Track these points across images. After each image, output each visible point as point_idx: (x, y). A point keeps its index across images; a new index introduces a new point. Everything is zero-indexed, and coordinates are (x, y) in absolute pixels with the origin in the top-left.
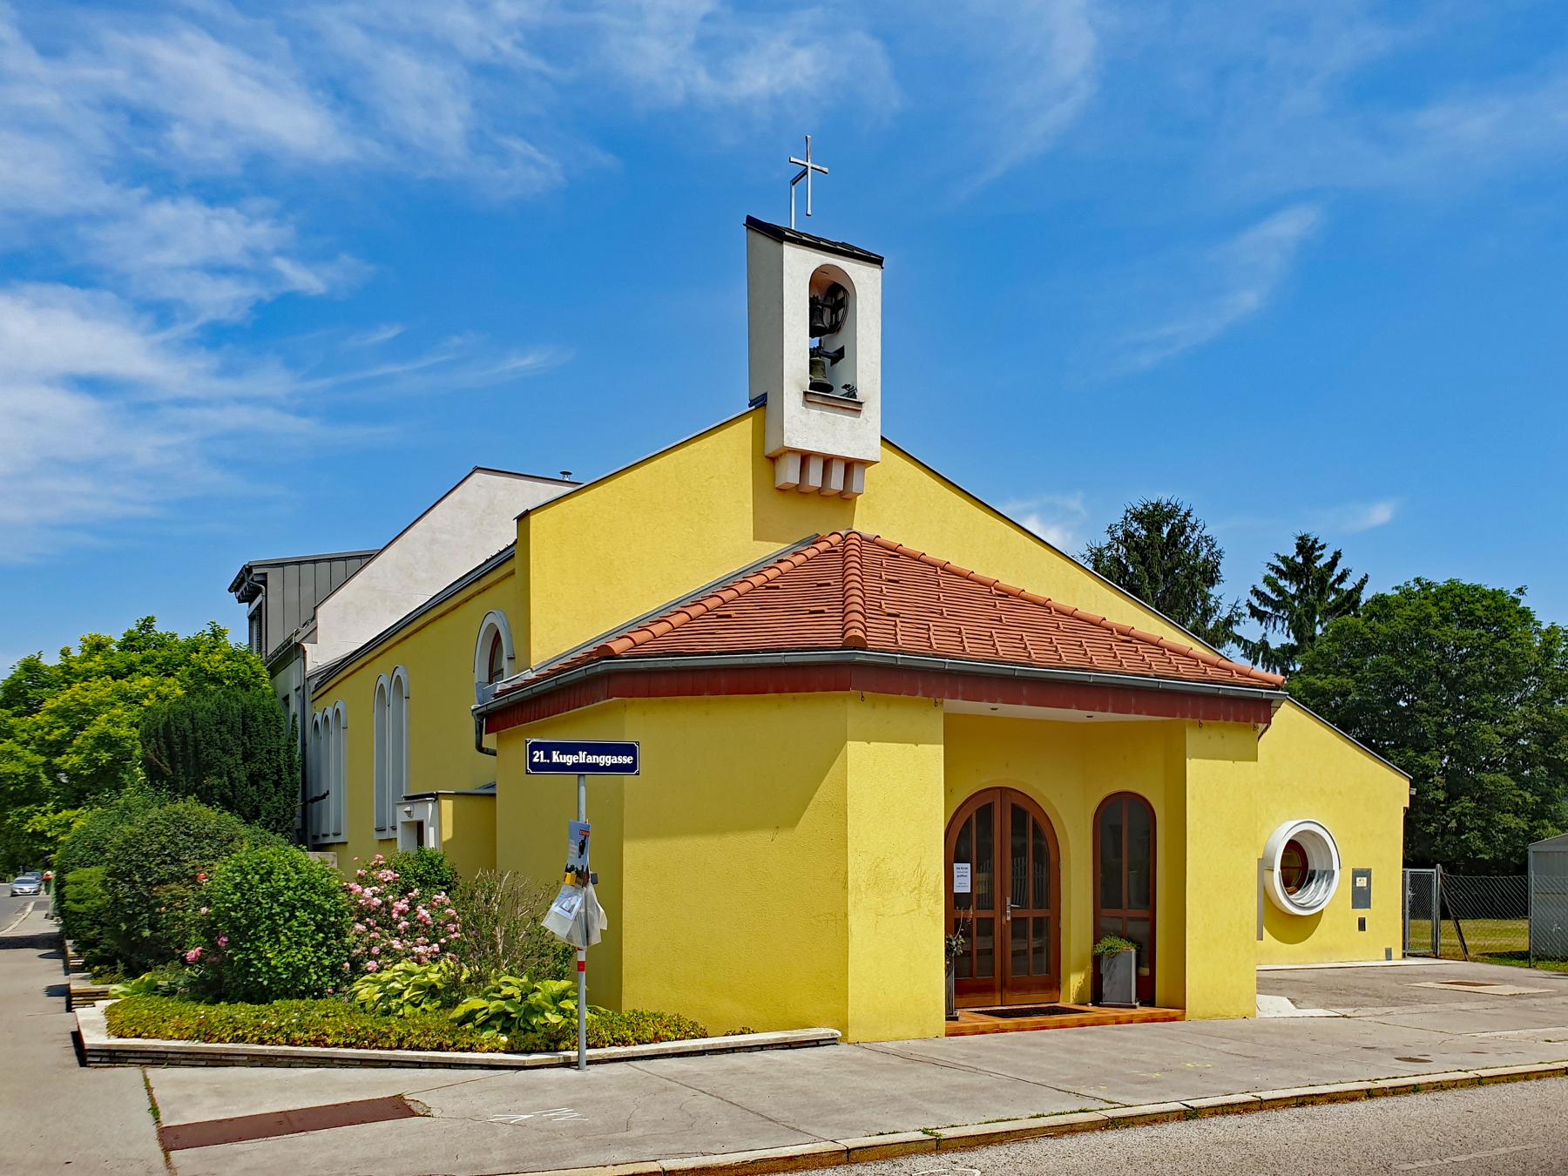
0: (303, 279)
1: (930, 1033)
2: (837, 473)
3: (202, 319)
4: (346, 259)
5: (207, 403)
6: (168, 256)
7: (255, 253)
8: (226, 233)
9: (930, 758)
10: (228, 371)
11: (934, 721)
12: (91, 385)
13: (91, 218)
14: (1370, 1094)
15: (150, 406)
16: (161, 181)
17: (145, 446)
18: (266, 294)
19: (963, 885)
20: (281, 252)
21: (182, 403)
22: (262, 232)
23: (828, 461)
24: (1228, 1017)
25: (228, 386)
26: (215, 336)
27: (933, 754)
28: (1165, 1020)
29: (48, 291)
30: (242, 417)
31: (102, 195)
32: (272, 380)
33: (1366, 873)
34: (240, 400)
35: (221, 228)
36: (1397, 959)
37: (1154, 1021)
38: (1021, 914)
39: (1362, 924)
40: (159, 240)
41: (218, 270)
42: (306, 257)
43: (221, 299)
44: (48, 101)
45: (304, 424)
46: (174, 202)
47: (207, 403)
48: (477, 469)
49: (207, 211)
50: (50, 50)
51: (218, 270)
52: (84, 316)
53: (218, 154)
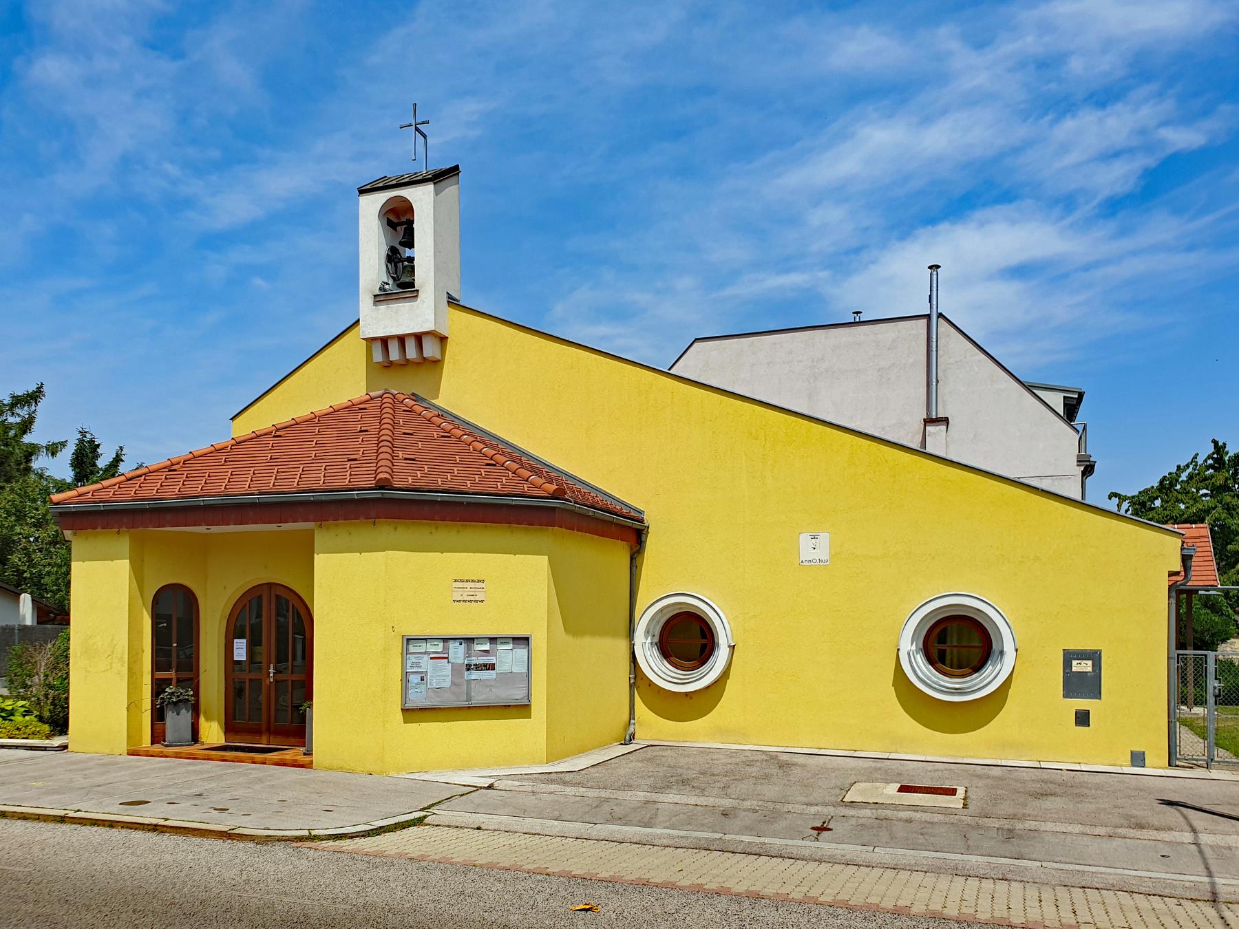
0: (1183, 138)
1: (117, 752)
2: (411, 347)
3: (1100, 198)
4: (1225, 108)
5: (1107, 262)
6: (1072, 158)
7: (1143, 132)
8: (1117, 125)
9: (122, 568)
10: (1123, 232)
11: (123, 543)
12: (1019, 271)
13: (1016, 150)
14: (63, 819)
15: (1065, 276)
16: (1061, 105)
17: (1062, 307)
18: (1150, 161)
19: (240, 653)
20: (1164, 124)
21: (1087, 268)
22: (1147, 113)
23: (401, 339)
24: (352, 772)
25: (1127, 244)
26: (1113, 206)
27: (124, 566)
28: (294, 766)
29: (987, 213)
30: (1138, 266)
31: (1021, 131)
32: (1162, 227)
33: (1095, 656)
34: (1134, 253)
35: (1112, 122)
36: (1156, 764)
37: (285, 765)
38: (281, 677)
39: (1083, 718)
40: (1064, 148)
41: (1111, 155)
42: (1185, 119)
43: (1116, 177)
44: (981, 79)
45: (1193, 258)
46: (1073, 117)
47: (1107, 262)
48: (696, 340)
49: (1100, 113)
50: (980, 45)
51: (1111, 155)
52: (1013, 222)
53: (1108, 65)
